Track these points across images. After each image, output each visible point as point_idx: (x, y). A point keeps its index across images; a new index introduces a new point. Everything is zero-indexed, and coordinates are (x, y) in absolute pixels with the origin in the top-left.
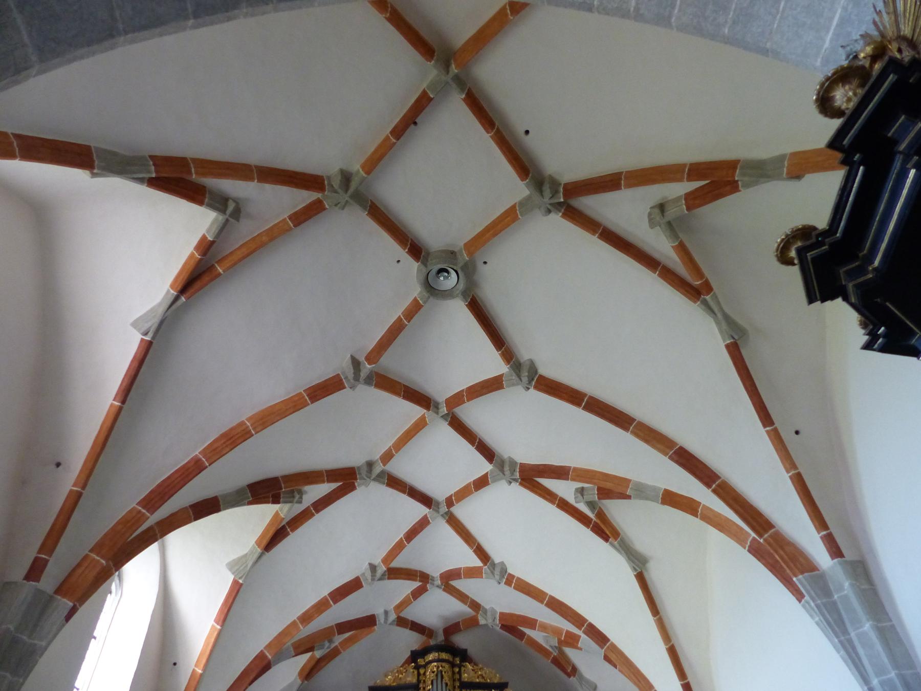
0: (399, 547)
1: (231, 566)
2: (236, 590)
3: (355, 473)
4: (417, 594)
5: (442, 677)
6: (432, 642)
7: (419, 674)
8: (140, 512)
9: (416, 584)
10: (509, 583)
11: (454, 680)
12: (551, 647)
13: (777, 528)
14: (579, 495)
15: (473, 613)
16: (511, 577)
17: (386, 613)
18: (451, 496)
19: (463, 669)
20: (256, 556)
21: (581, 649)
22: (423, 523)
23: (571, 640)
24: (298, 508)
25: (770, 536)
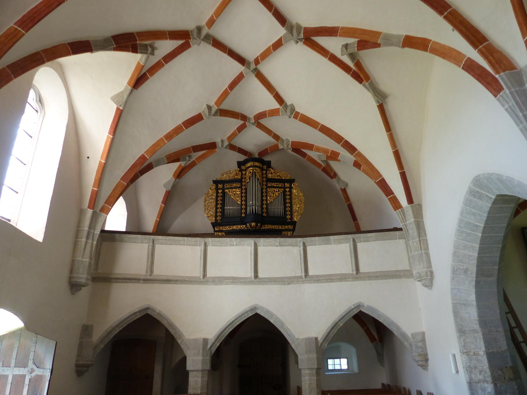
0: (225, 95)
1: (114, 99)
2: (119, 116)
3: (189, 34)
4: (241, 129)
7: (242, 174)
8: (16, 29)
9: (240, 122)
10: (296, 117)
11: (263, 178)
13: (490, 41)
14: (344, 48)
16: (297, 113)
17: (222, 141)
18: (258, 57)
19: (268, 172)
20: (128, 92)
21: (339, 161)
22: (240, 77)
23: (334, 156)
24: (154, 60)
25: (484, 47)
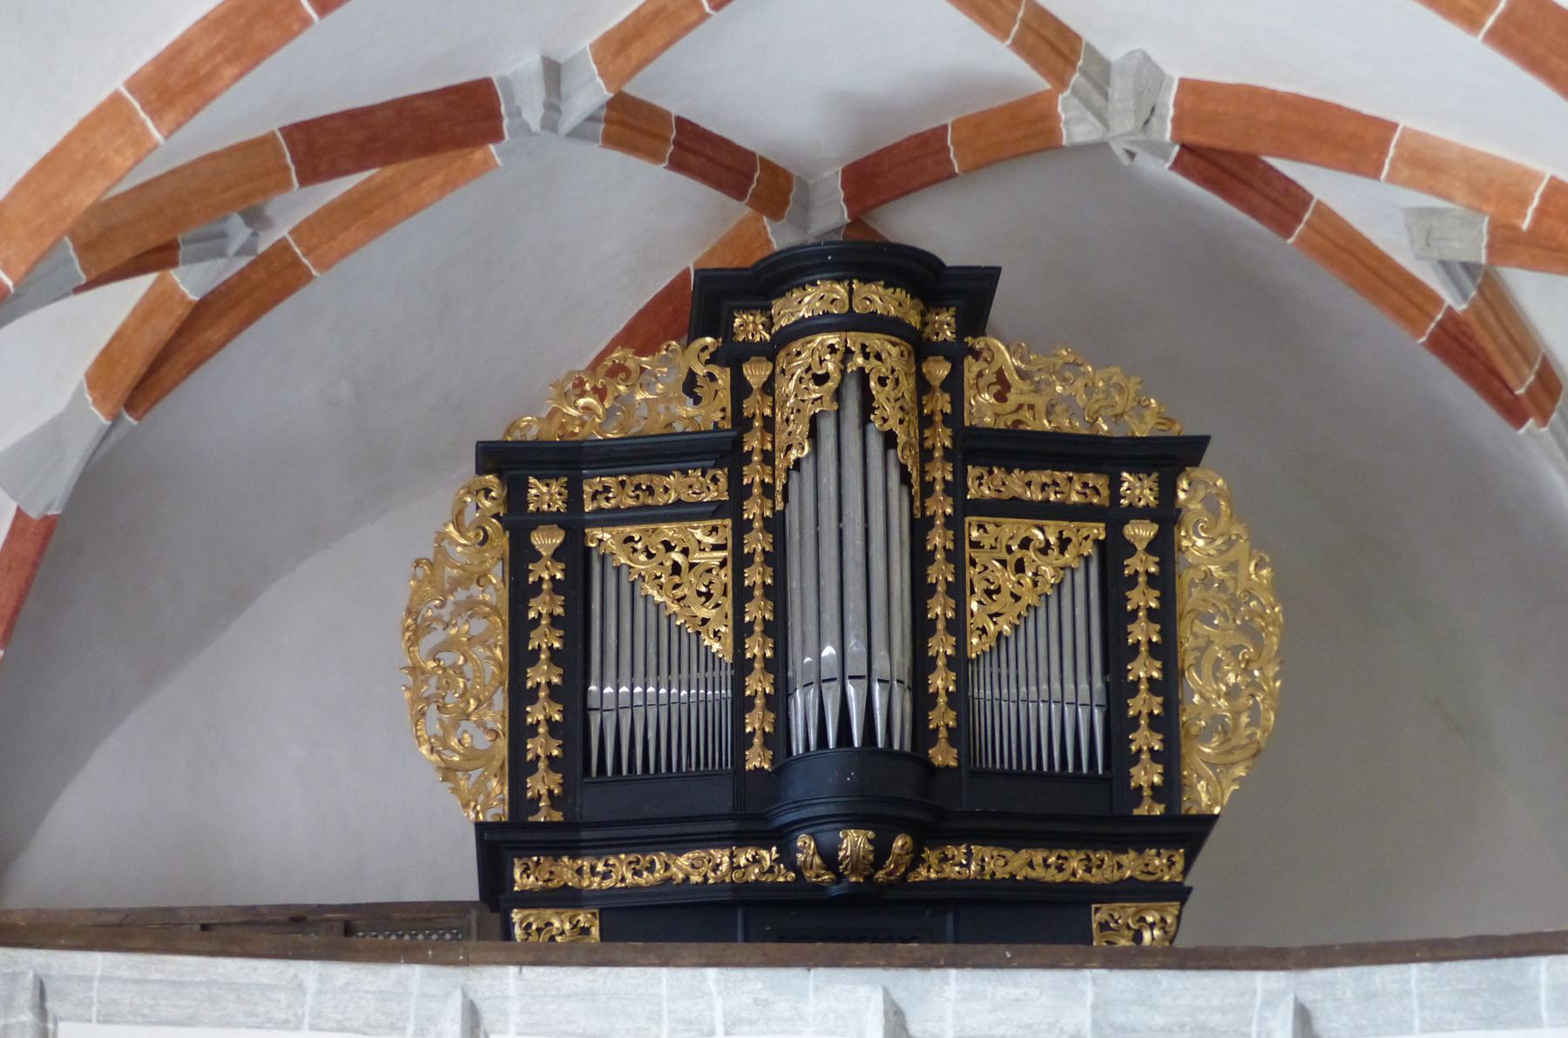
5: (867, 405)
6: (780, 236)
7: (740, 389)
11: (925, 422)
12: (1445, 265)
15: (1042, 84)
17: (553, 72)
19: (971, 367)
